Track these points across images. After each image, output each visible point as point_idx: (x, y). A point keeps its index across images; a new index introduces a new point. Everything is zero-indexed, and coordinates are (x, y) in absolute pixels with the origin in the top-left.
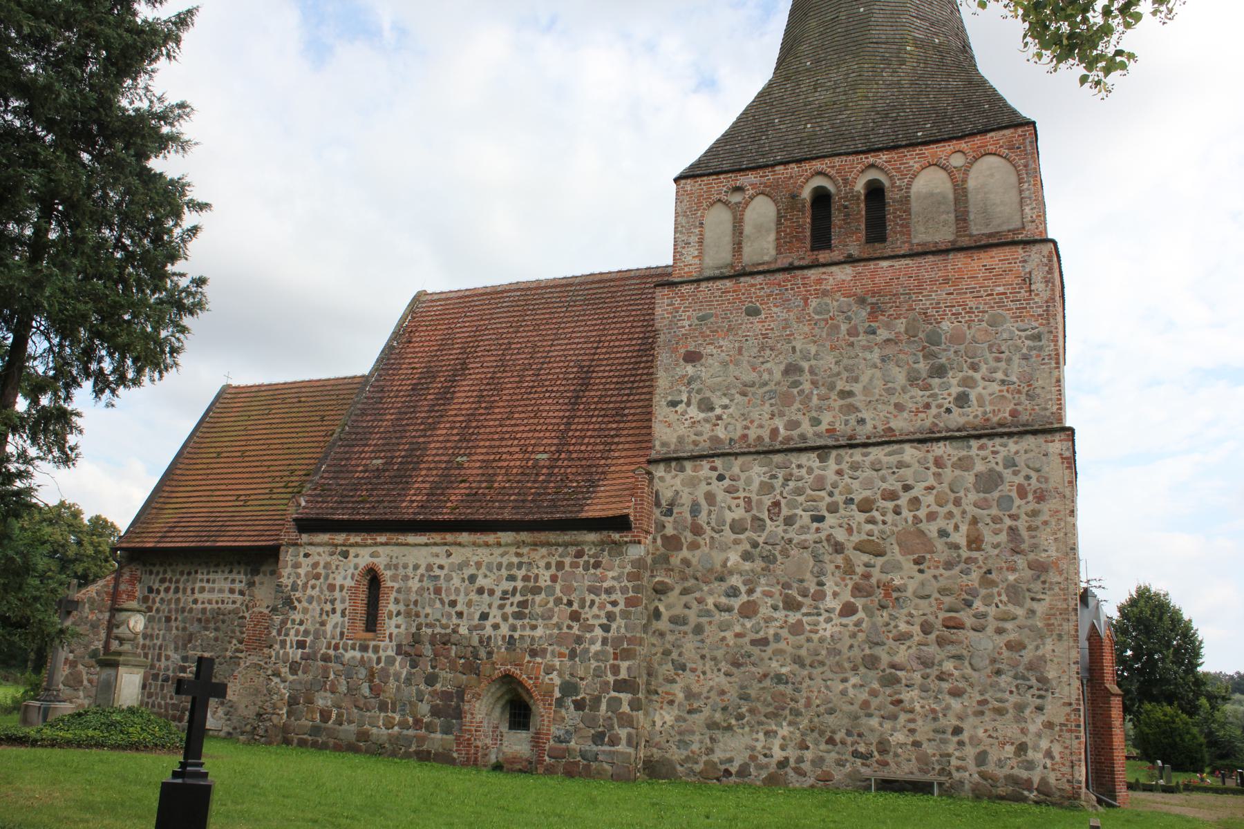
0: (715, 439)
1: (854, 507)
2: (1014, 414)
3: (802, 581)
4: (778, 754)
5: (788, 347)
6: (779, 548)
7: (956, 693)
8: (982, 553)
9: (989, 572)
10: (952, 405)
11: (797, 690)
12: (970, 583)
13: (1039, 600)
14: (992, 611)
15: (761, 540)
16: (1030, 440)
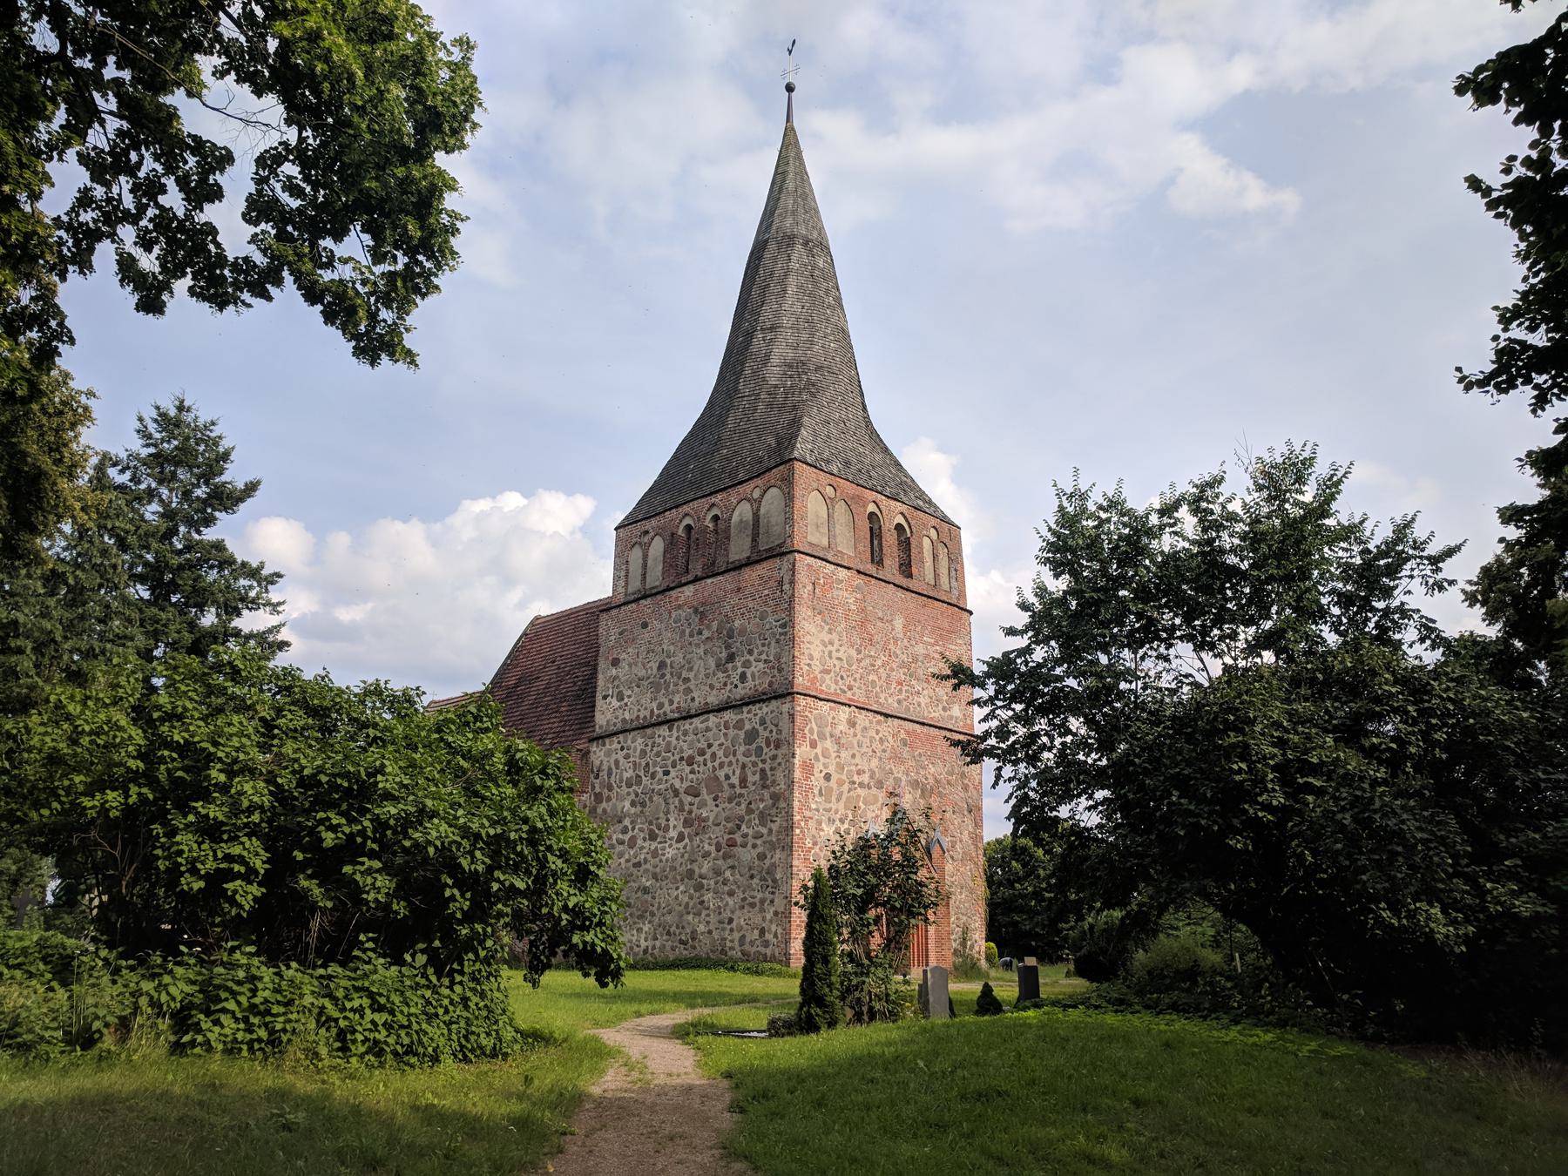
0: (624, 720)
2: (771, 684)
4: (643, 944)
7: (731, 894)
9: (750, 803)
11: (654, 898)
16: (774, 703)
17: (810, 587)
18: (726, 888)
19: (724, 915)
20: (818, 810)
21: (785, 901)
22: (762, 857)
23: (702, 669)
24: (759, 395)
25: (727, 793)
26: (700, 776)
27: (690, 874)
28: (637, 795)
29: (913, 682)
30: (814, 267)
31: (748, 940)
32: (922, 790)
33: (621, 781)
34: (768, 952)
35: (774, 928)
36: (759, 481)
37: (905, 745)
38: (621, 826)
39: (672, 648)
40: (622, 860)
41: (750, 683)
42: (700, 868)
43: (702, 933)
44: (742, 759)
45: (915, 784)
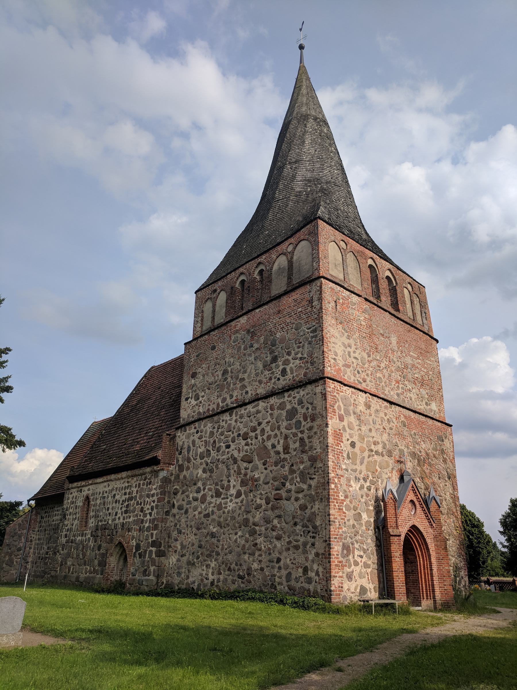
0: (199, 413)
1: (241, 438)
2: (305, 375)
3: (222, 481)
4: (211, 577)
5: (224, 362)
6: (215, 464)
7: (279, 538)
8: (289, 455)
9: (292, 465)
10: (280, 376)
11: (218, 541)
12: (284, 473)
13: (313, 479)
14: (293, 487)
15: (209, 461)
16: (309, 387)
17: (333, 304)
18: (275, 534)
19: (273, 555)
20: (347, 470)
21: (324, 544)
22: (303, 508)
23: (253, 371)
24: (289, 197)
25: (274, 458)
26: (252, 447)
27: (246, 522)
28: (207, 464)
29: (406, 382)
30: (322, 131)
31: (293, 576)
32: (418, 460)
33: (196, 455)
34: (311, 587)
35: (315, 567)
36: (292, 240)
37: (405, 426)
38: (196, 487)
39: (232, 360)
40: (196, 513)
41: (289, 376)
42: (254, 517)
43: (256, 570)
44: (284, 430)
45: (413, 455)
